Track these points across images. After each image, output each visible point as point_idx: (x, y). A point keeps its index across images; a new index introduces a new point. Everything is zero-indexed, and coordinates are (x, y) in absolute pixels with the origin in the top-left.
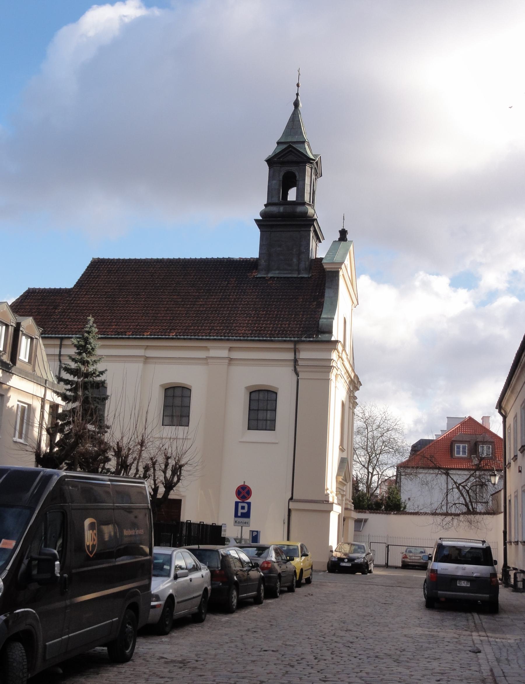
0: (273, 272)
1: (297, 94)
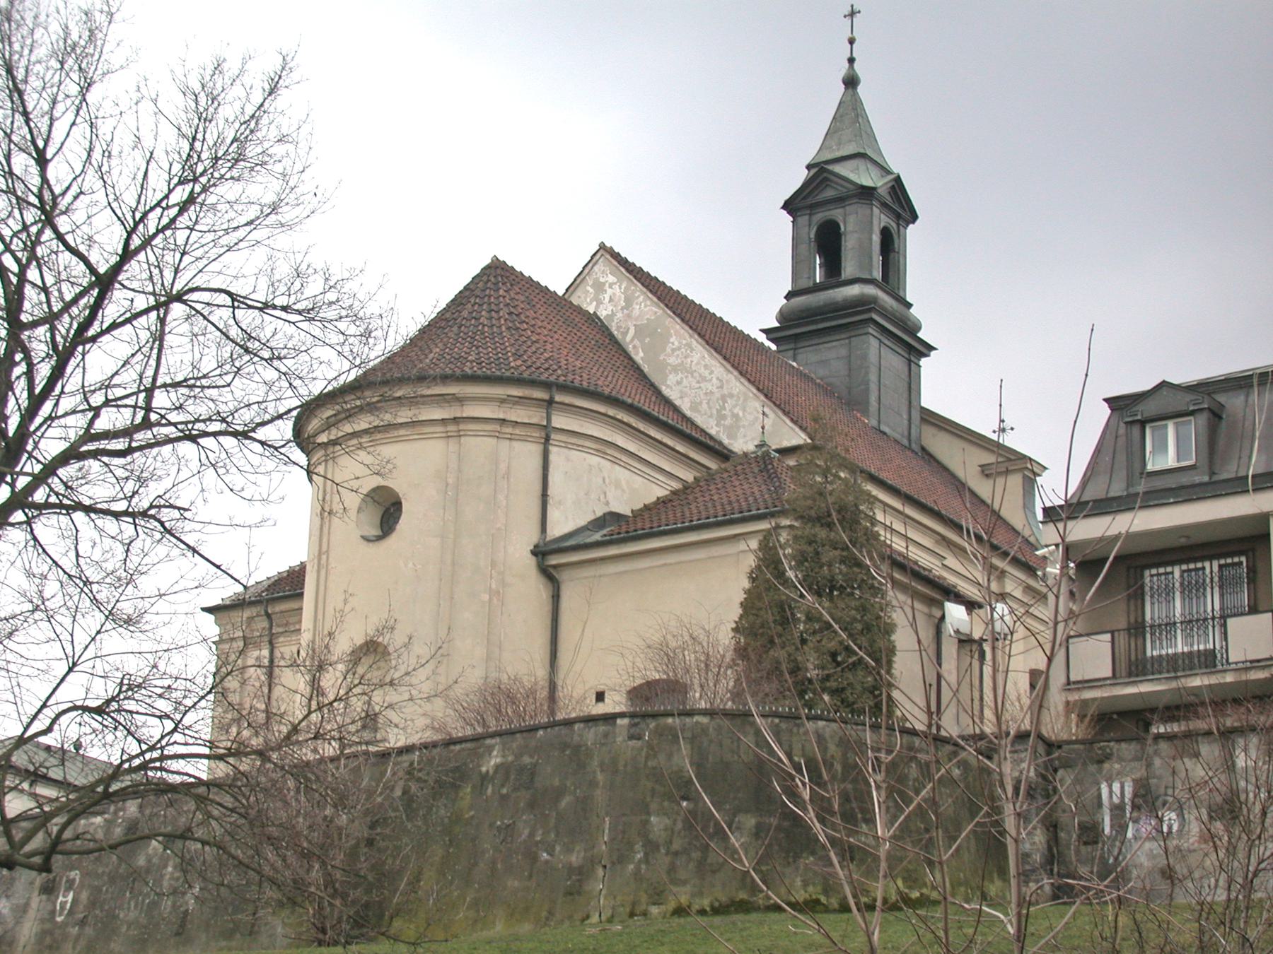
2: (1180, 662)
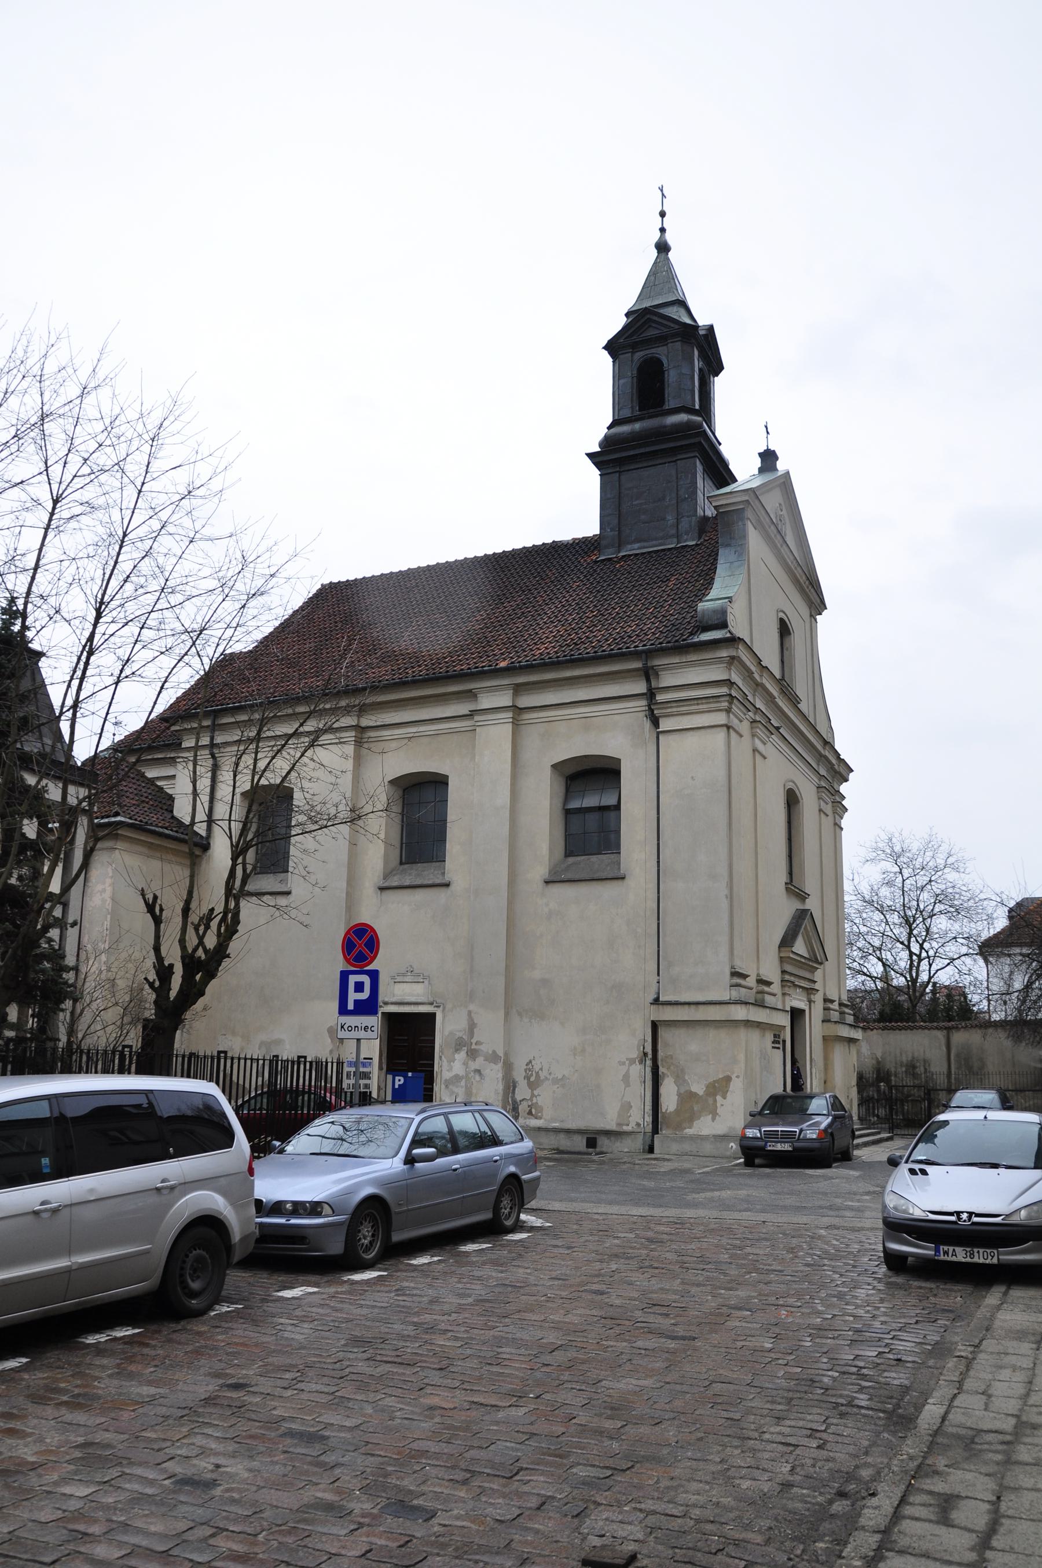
0: (629, 546)
2: (100, 1067)
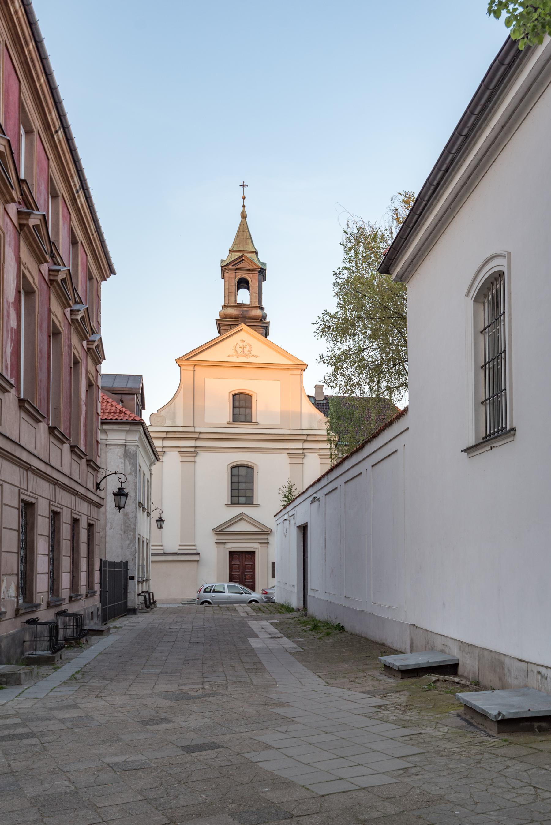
1: (244, 206)
